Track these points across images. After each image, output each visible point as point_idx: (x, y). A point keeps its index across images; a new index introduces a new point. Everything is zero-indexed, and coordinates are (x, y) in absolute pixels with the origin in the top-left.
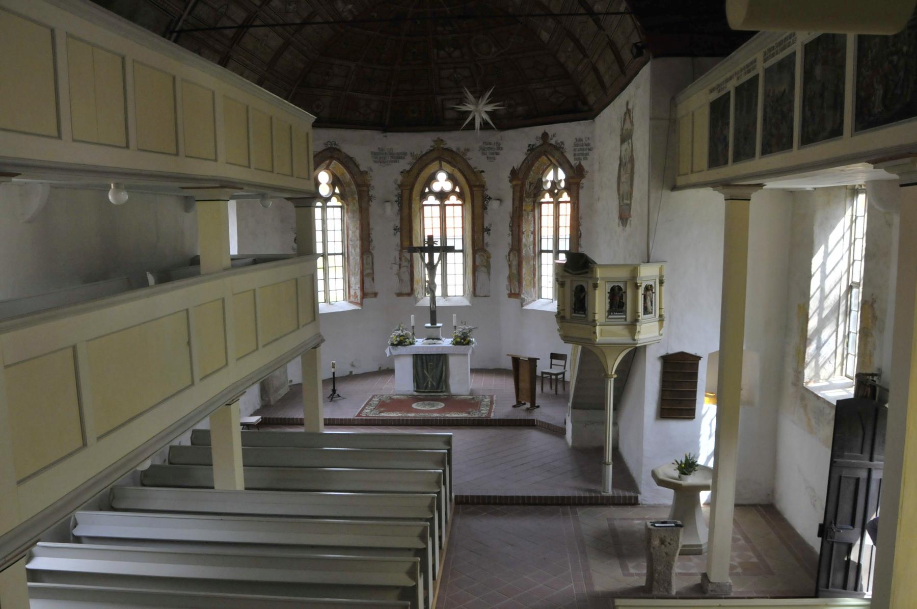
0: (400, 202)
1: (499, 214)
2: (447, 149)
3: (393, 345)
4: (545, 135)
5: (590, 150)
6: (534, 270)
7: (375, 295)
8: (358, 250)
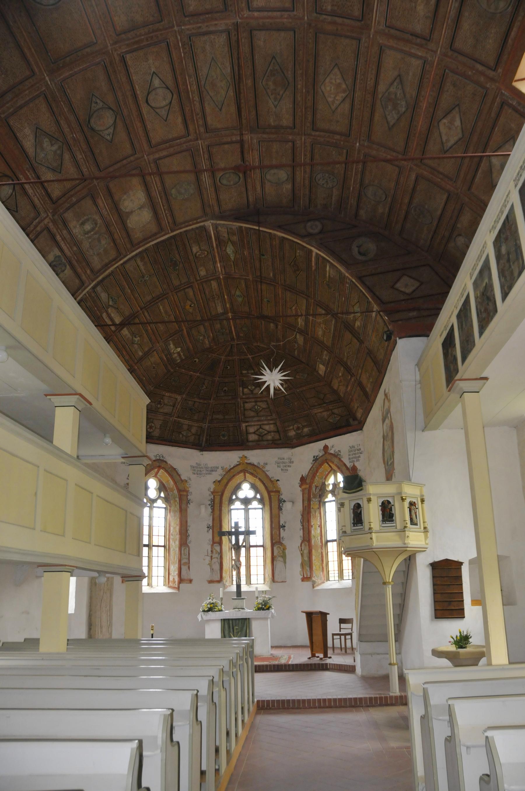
0: (213, 506)
1: (292, 512)
2: (250, 464)
3: (204, 611)
4: (326, 447)
5: (361, 453)
6: (322, 557)
7: (191, 581)
8: (177, 543)
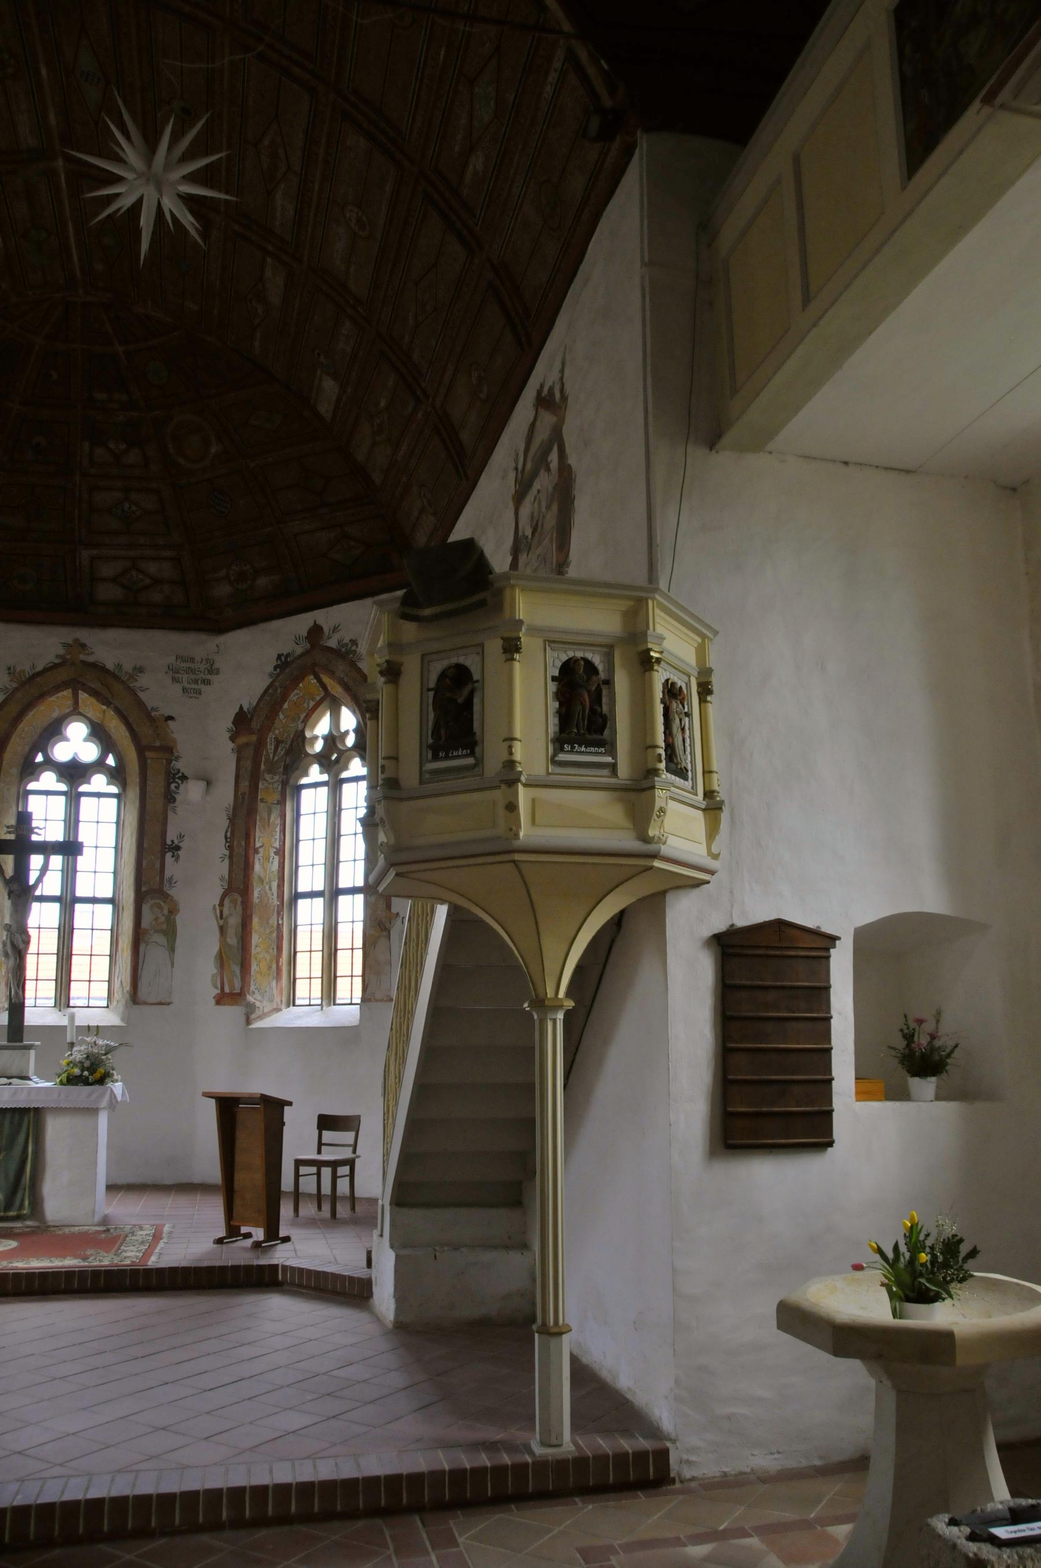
1: (202, 811)
2: (94, 665)
4: (316, 632)
6: (280, 938)
